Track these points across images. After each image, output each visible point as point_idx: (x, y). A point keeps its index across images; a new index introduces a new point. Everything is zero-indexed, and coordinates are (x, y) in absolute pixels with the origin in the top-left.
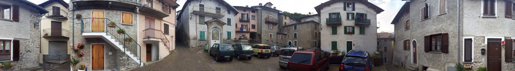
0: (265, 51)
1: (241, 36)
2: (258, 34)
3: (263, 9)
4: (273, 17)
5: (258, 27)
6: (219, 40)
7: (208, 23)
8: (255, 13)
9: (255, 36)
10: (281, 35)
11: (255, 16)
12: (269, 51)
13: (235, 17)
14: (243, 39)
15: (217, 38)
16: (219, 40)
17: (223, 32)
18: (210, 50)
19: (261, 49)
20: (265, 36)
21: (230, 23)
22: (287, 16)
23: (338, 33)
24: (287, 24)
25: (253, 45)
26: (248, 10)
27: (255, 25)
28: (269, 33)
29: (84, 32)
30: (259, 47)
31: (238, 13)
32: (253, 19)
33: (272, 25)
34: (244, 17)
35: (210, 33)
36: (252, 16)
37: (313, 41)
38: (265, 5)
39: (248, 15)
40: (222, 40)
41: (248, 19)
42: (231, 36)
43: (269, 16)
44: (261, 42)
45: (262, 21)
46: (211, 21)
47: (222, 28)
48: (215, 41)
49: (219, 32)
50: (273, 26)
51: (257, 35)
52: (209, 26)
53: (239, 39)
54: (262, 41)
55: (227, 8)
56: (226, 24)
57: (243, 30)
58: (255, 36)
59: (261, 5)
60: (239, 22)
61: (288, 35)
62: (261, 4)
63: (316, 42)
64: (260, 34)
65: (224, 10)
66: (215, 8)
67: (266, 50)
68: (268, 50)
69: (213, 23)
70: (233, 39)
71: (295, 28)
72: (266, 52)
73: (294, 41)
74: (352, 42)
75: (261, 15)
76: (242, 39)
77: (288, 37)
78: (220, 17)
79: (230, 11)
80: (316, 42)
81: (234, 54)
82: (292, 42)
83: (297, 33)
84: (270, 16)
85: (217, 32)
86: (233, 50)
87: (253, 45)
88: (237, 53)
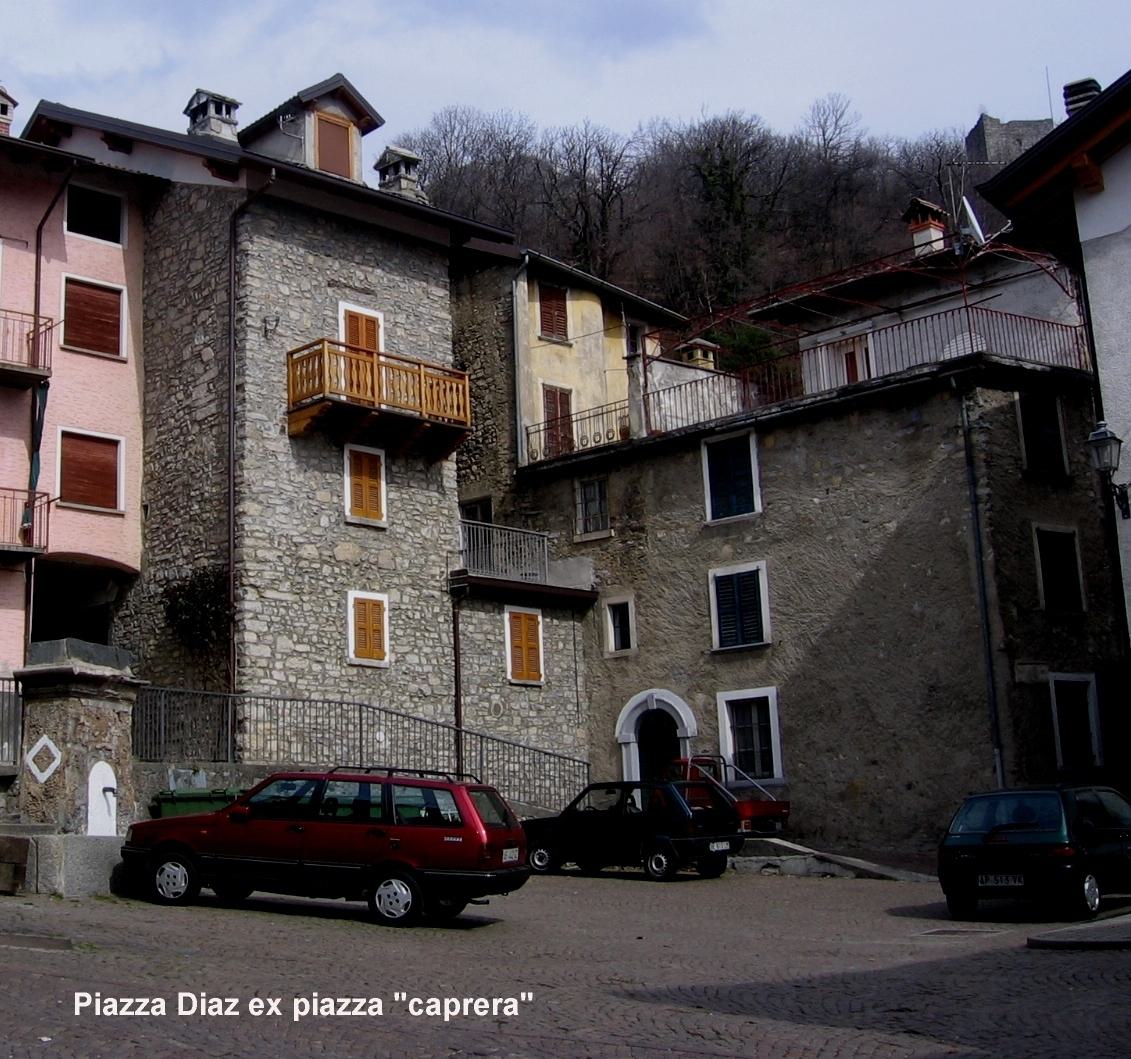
8: (117, 240)
10: (508, 609)
22: (583, 287)
24: (588, 434)
29: (495, 818)
36: (65, 434)
37: (1023, 673)
54: (253, 711)
61: (620, 612)
63: (1071, 694)
71: (732, 493)
73: (723, 697)
77: (623, 640)
80: (1071, 694)
82: (689, 721)
83: (760, 565)
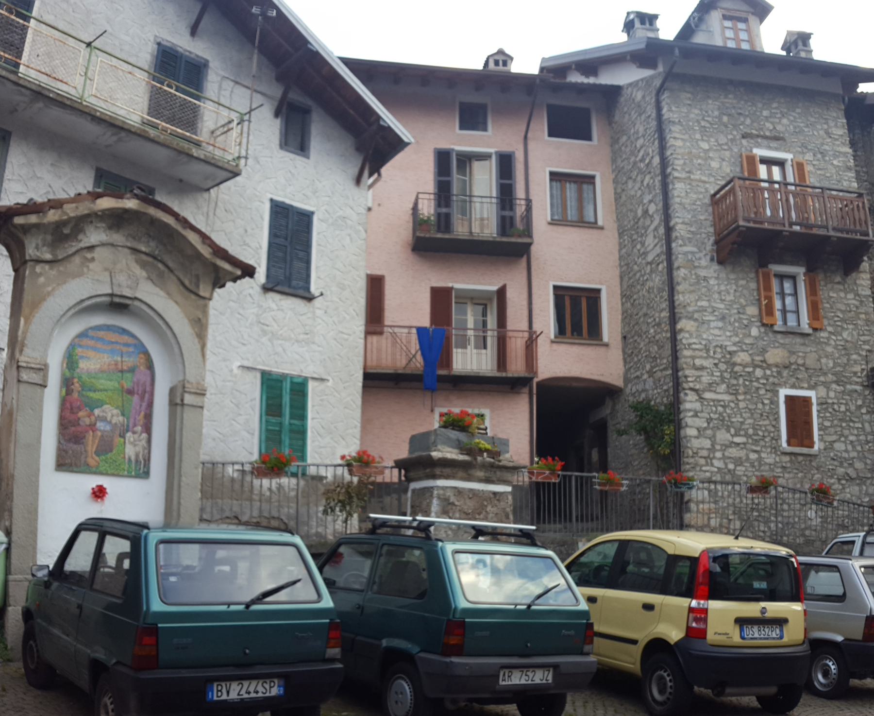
0: (742, 622)
1: (426, 435)
2: (635, 408)
3: (670, 76)
4: (800, 168)
5: (627, 317)
6: (142, 470)
7: (26, 229)
8: (586, 136)
9: (602, 429)
11: (590, 180)
12: (780, 622)
13: (366, 197)
14: (449, 467)
15: (130, 451)
16: (146, 474)
17: (209, 381)
18: (27, 615)
19: (688, 593)
20: (724, 423)
21: (298, 265)
25: (574, 546)
26: (506, 111)
27: (593, 296)
30: (660, 565)
31: (394, 145)
32: (572, 214)
33: (800, 271)
34: (468, 196)
35: (43, 369)
38: (687, 31)
39: (505, 163)
40: (192, 477)
41: (506, 224)
42: (300, 433)
43: (751, 160)
44: (682, 505)
45: (681, 230)
46: (71, 211)
47: (200, 326)
48: (99, 493)
49: (150, 367)
50: (812, 291)
51: (632, 416)
52: (42, 276)
53: (400, 464)
55: (279, 79)
56: (249, 271)
57: (447, 361)
58: (601, 430)
59: (642, 33)
60: (412, 257)
62: (648, 20)
64: (658, 398)
65: (241, 99)
66: (146, 56)
67: (751, 609)
68: (775, 608)
69: (94, 236)
70: (329, 474)
72: (754, 632)
75: (664, 163)
76: (445, 463)
78: (194, 172)
79: (306, 112)
81: (334, 652)
84: (769, 162)
85: (129, 361)
86: (327, 602)
87: (582, 547)
88: (384, 643)
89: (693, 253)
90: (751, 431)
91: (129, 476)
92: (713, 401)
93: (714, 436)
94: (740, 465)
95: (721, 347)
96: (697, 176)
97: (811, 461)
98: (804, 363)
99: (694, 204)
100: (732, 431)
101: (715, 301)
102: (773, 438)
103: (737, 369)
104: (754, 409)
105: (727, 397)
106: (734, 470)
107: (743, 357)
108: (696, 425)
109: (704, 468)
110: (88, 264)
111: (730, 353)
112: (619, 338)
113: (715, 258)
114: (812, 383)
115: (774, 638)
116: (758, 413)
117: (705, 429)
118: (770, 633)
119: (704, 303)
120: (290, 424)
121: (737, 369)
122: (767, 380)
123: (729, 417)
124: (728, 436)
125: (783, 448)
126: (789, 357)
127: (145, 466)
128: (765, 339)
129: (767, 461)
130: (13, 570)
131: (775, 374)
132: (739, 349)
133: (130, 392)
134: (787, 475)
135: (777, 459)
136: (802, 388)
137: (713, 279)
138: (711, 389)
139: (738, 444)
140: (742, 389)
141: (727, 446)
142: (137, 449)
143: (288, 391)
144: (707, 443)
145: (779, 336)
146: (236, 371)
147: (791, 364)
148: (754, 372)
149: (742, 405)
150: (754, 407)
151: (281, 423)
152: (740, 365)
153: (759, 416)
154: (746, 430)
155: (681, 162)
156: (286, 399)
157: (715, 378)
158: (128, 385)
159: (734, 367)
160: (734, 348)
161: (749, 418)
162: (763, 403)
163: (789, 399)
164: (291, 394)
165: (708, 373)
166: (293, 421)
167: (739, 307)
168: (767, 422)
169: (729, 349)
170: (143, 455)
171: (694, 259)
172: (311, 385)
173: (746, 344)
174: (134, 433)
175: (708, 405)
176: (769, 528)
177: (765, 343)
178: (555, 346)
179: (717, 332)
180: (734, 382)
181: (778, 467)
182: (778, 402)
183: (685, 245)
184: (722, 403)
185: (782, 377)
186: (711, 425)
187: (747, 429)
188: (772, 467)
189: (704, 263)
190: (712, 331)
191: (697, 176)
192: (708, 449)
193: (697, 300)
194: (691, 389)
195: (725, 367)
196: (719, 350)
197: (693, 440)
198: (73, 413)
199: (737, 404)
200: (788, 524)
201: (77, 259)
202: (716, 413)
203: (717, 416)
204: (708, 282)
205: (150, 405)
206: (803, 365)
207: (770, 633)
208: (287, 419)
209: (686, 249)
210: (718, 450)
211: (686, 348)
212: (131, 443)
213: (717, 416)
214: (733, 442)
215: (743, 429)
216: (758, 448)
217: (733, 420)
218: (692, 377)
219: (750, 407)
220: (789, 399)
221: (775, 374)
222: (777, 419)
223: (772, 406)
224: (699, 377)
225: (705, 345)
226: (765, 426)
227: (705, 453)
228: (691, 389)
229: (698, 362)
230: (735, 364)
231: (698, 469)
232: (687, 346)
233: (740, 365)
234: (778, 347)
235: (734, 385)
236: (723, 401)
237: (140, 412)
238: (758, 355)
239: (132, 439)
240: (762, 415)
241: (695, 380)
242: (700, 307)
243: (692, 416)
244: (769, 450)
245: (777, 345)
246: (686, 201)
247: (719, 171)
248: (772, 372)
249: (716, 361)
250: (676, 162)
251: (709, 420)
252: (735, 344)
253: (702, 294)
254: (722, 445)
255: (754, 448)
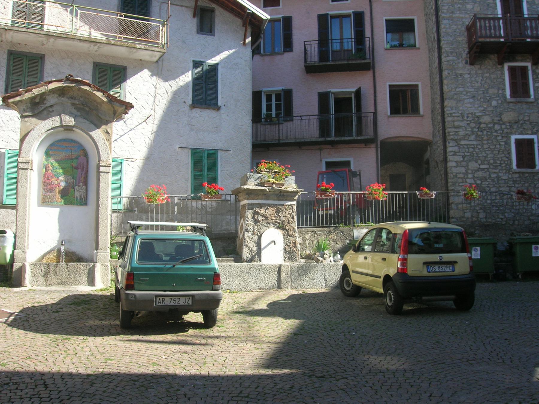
12: (453, 263)
15: (77, 194)
23: (43, 53)
27: (414, 89)
28: (509, 138)
67: (435, 257)
74: (386, 20)
85: (75, 154)
89: (453, 60)
90: (492, 161)
91: (77, 205)
92: (467, 145)
93: (467, 165)
94: (484, 181)
95: (472, 114)
96: (457, 14)
97: (534, 176)
98: (529, 119)
99: (455, 31)
100: (479, 162)
101: (468, 87)
102: (507, 164)
103: (482, 126)
104: (494, 148)
105: (475, 143)
106: (481, 184)
107: (486, 119)
108: (455, 160)
109: (461, 184)
110: (51, 114)
111: (478, 117)
112: (430, 111)
113: (468, 62)
114: (534, 131)
115: (448, 272)
116: (496, 151)
117: (461, 161)
118: (446, 269)
119: (461, 89)
120: (208, 175)
121: (482, 126)
122: (503, 131)
123: (477, 154)
124: (477, 165)
125: (515, 170)
126: (518, 117)
127: (84, 200)
128: (502, 107)
129: (504, 178)
130: (16, 247)
131: (508, 127)
132: (484, 114)
133: (76, 168)
134: (517, 185)
135: (510, 176)
136: (527, 134)
137: (467, 75)
138: (466, 138)
139: (483, 169)
140: (485, 138)
141: (476, 171)
142: (81, 193)
143: (206, 158)
144: (463, 170)
145: (511, 104)
146: (178, 149)
147: (519, 120)
148: (494, 127)
149: (485, 146)
150: (494, 147)
151: (202, 174)
152: (484, 123)
153: (497, 152)
154: (489, 161)
155: (447, 8)
156: (205, 162)
157: (468, 132)
158: (75, 164)
159: (480, 125)
160: (480, 114)
161: (490, 154)
162: (500, 145)
163: (517, 141)
164: (207, 159)
165: (463, 129)
166: (209, 173)
167: (483, 89)
168: (503, 155)
169: (477, 115)
170: (84, 196)
171: (454, 64)
172: (220, 154)
173: (488, 111)
174: (79, 186)
175: (464, 148)
176: (505, 216)
177: (502, 109)
178: (390, 119)
179: (469, 105)
180: (480, 133)
181: (510, 181)
182: (510, 143)
183: (448, 56)
184: (472, 146)
185: (513, 129)
186: (465, 159)
187: (490, 160)
188: (506, 181)
189: (460, 65)
190: (466, 105)
191: (457, 14)
192: (463, 173)
193: (456, 88)
194: (452, 139)
195: (474, 125)
196: (470, 116)
197: (453, 169)
198: (49, 179)
199: (482, 146)
200: (518, 214)
201: (45, 112)
202: (468, 152)
203: (469, 154)
204: (463, 77)
205: (87, 173)
206: (528, 120)
207: (446, 269)
208: (205, 172)
209: (448, 58)
210: (470, 173)
211: (448, 116)
212: (78, 191)
213: (469, 154)
214: (480, 168)
215: (487, 161)
216: (497, 171)
217: (480, 155)
218: (453, 132)
219: (491, 147)
220: (517, 141)
221: (508, 127)
222: (509, 153)
223: (506, 146)
224: (457, 132)
225: (461, 114)
226: (501, 157)
227: (461, 176)
228: (452, 139)
229: (456, 124)
230: (480, 123)
231: (457, 184)
232: (449, 115)
233: (484, 123)
234: (511, 111)
235: (480, 135)
236: (473, 145)
237: (82, 177)
238: (497, 117)
239: (78, 189)
240: (499, 151)
241: (455, 134)
242: (458, 91)
243: (453, 155)
244: (504, 171)
245: (509, 110)
246: (449, 31)
247: (472, 10)
248: (506, 126)
249: (468, 122)
250: (443, 8)
251: (464, 157)
252: (481, 112)
253: (459, 84)
254: (472, 170)
255: (496, 171)
